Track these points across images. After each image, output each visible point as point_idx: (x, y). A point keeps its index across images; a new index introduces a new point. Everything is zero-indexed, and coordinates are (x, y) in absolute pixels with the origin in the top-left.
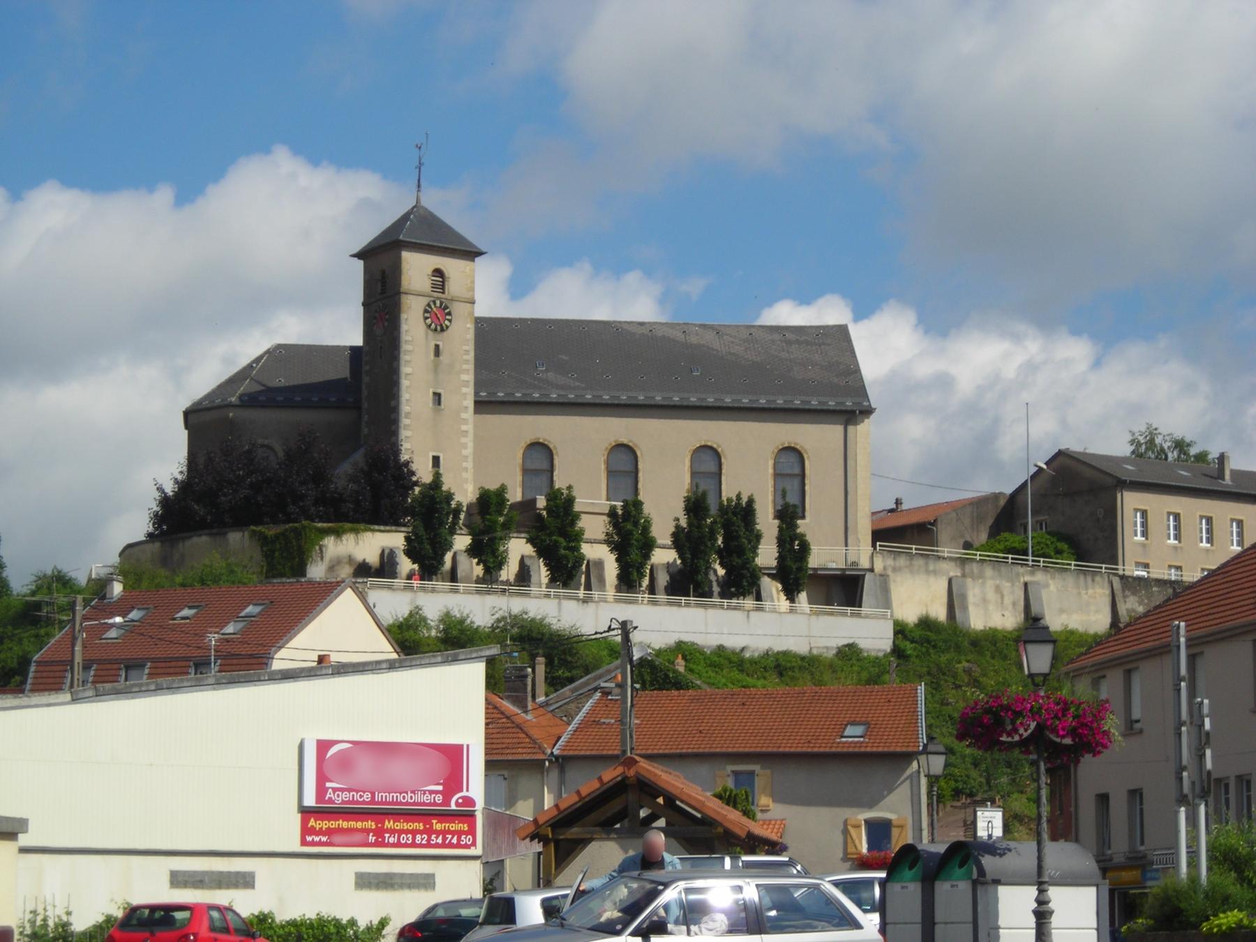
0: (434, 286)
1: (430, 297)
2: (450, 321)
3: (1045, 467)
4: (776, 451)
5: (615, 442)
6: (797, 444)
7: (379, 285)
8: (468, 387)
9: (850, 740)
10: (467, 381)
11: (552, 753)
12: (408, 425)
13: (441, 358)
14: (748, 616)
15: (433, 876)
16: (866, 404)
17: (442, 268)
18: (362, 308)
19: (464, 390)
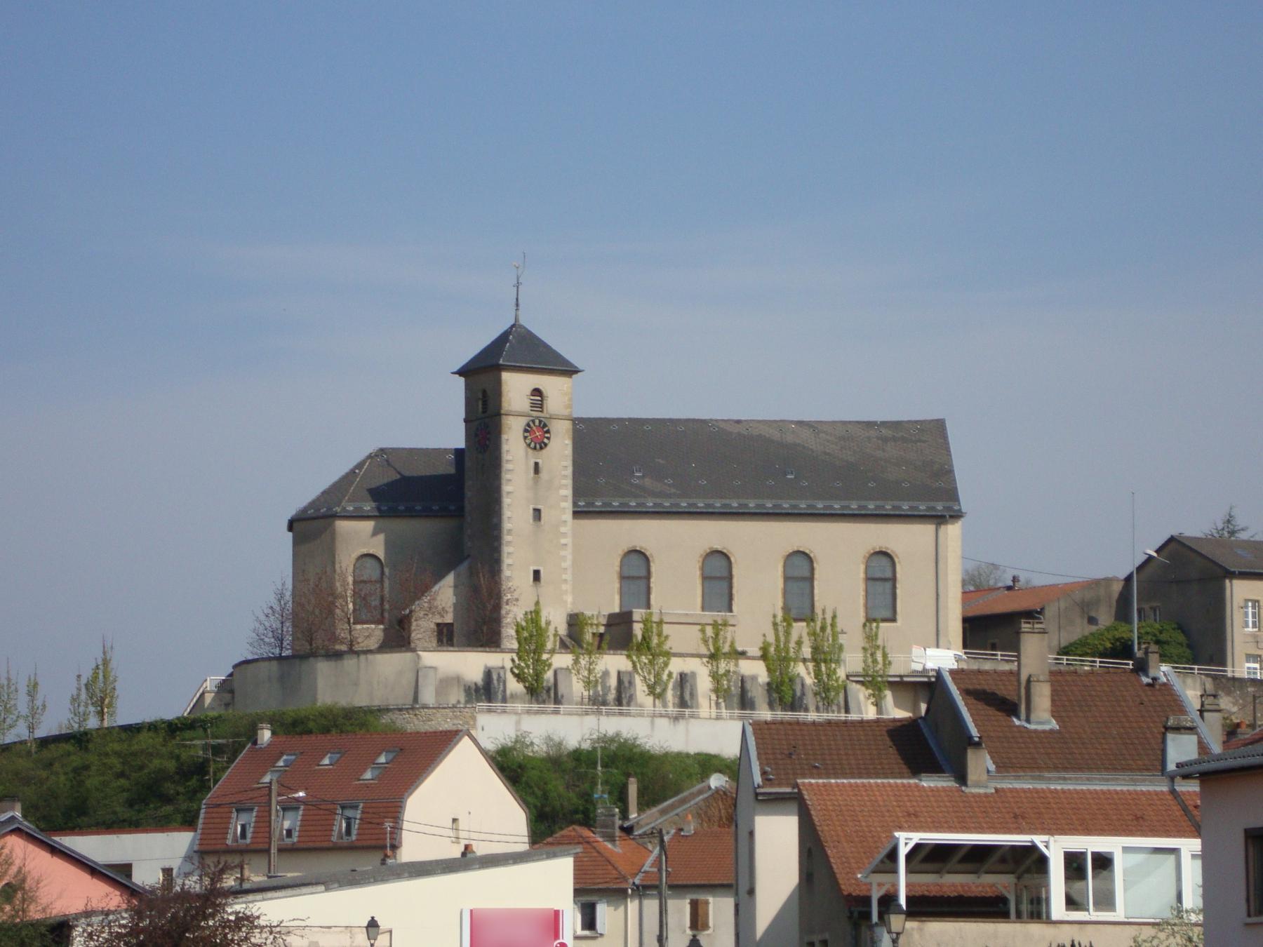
0: (533, 405)
2: (548, 438)
3: (1155, 554)
4: (867, 555)
5: (710, 549)
6: (888, 548)
7: (480, 403)
8: (566, 501)
10: (566, 496)
11: (634, 883)
12: (510, 542)
13: (541, 475)
16: (956, 508)
17: (541, 388)
18: (464, 424)
19: (563, 504)
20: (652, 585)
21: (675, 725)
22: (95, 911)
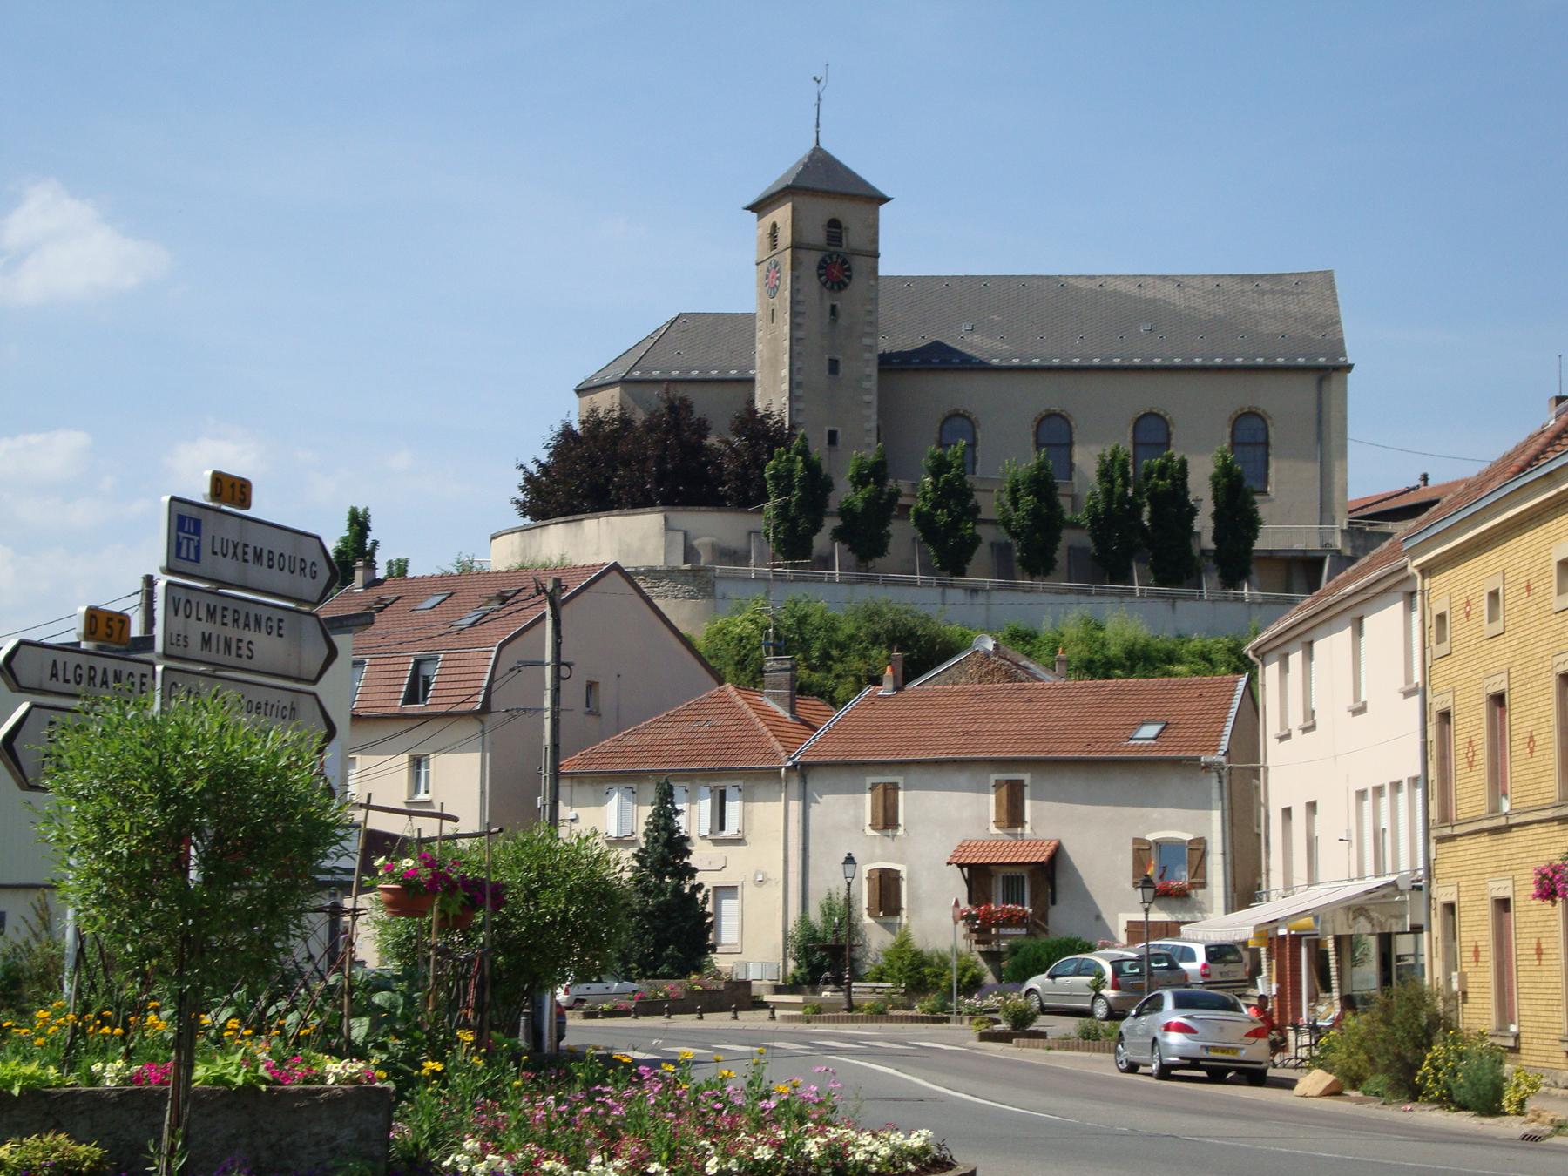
1: (825, 251)
9: (1140, 742)
12: (799, 397)
14: (1173, 607)
20: (977, 454)
21: (972, 598)
22: (803, 917)
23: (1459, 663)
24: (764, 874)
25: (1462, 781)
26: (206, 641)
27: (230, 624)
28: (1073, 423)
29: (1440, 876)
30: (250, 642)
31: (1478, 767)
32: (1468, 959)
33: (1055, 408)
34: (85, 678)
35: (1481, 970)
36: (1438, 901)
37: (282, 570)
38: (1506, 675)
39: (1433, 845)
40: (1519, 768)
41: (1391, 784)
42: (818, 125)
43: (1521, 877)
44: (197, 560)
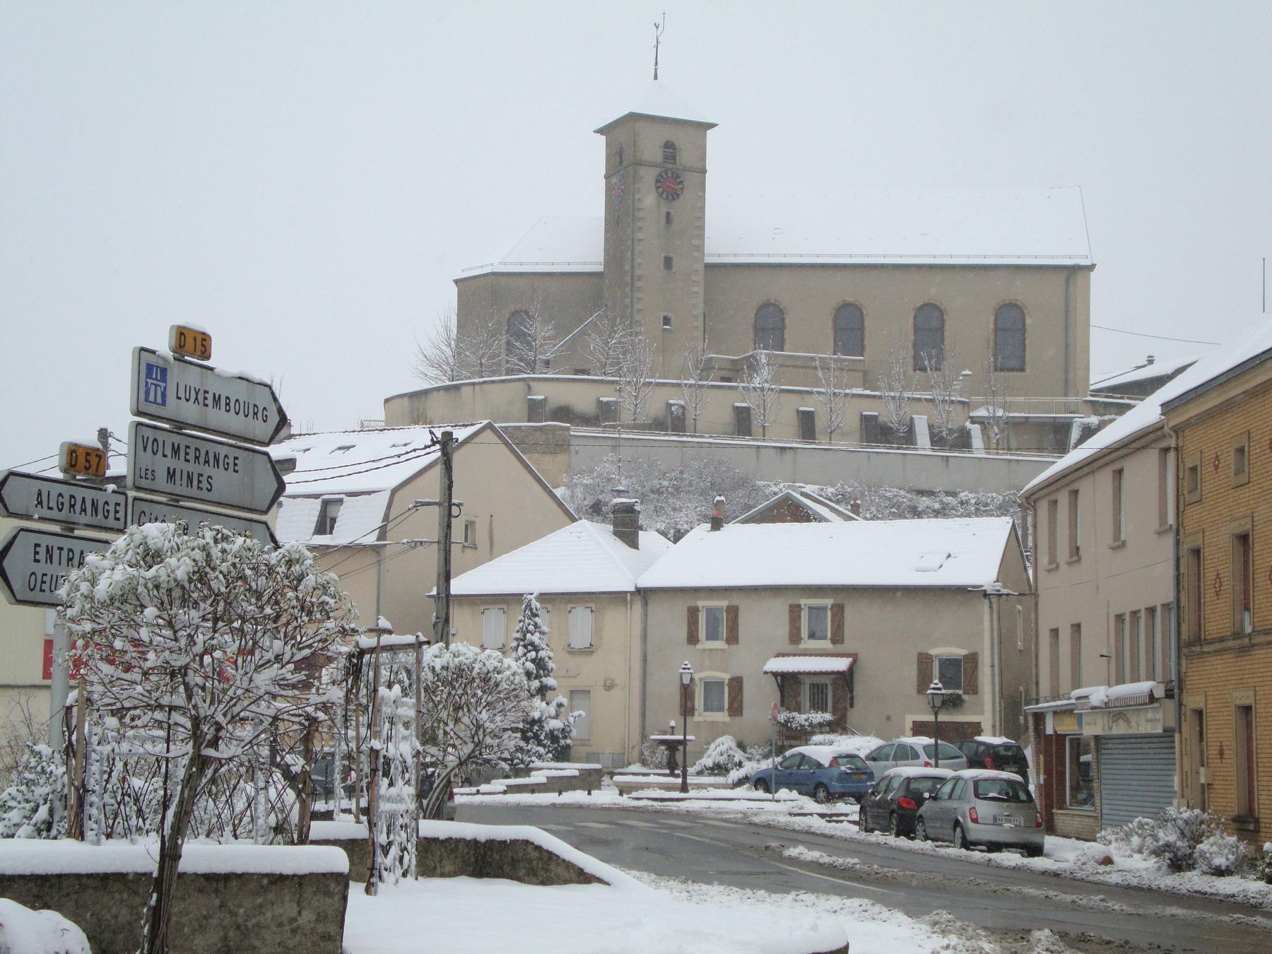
0: (666, 157)
15: (979, 724)
21: (782, 454)
23: (1208, 508)
24: (613, 681)
25: (1210, 607)
26: (171, 475)
27: (192, 461)
28: (865, 312)
29: (1189, 687)
30: (209, 477)
31: (1224, 596)
32: (1214, 757)
33: (850, 299)
34: (67, 506)
35: (1225, 765)
36: (1188, 708)
37: (237, 414)
38: (1250, 519)
39: (1184, 662)
40: (1261, 597)
41: (1146, 609)
42: (656, 64)
43: (1262, 688)
44: (164, 403)
